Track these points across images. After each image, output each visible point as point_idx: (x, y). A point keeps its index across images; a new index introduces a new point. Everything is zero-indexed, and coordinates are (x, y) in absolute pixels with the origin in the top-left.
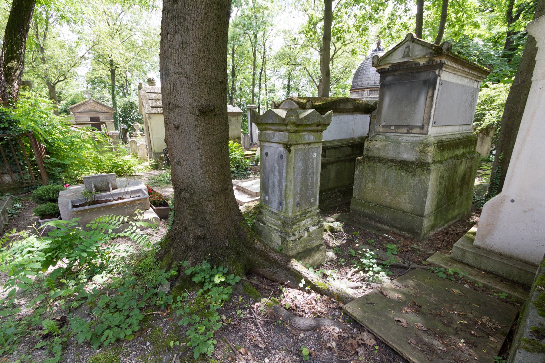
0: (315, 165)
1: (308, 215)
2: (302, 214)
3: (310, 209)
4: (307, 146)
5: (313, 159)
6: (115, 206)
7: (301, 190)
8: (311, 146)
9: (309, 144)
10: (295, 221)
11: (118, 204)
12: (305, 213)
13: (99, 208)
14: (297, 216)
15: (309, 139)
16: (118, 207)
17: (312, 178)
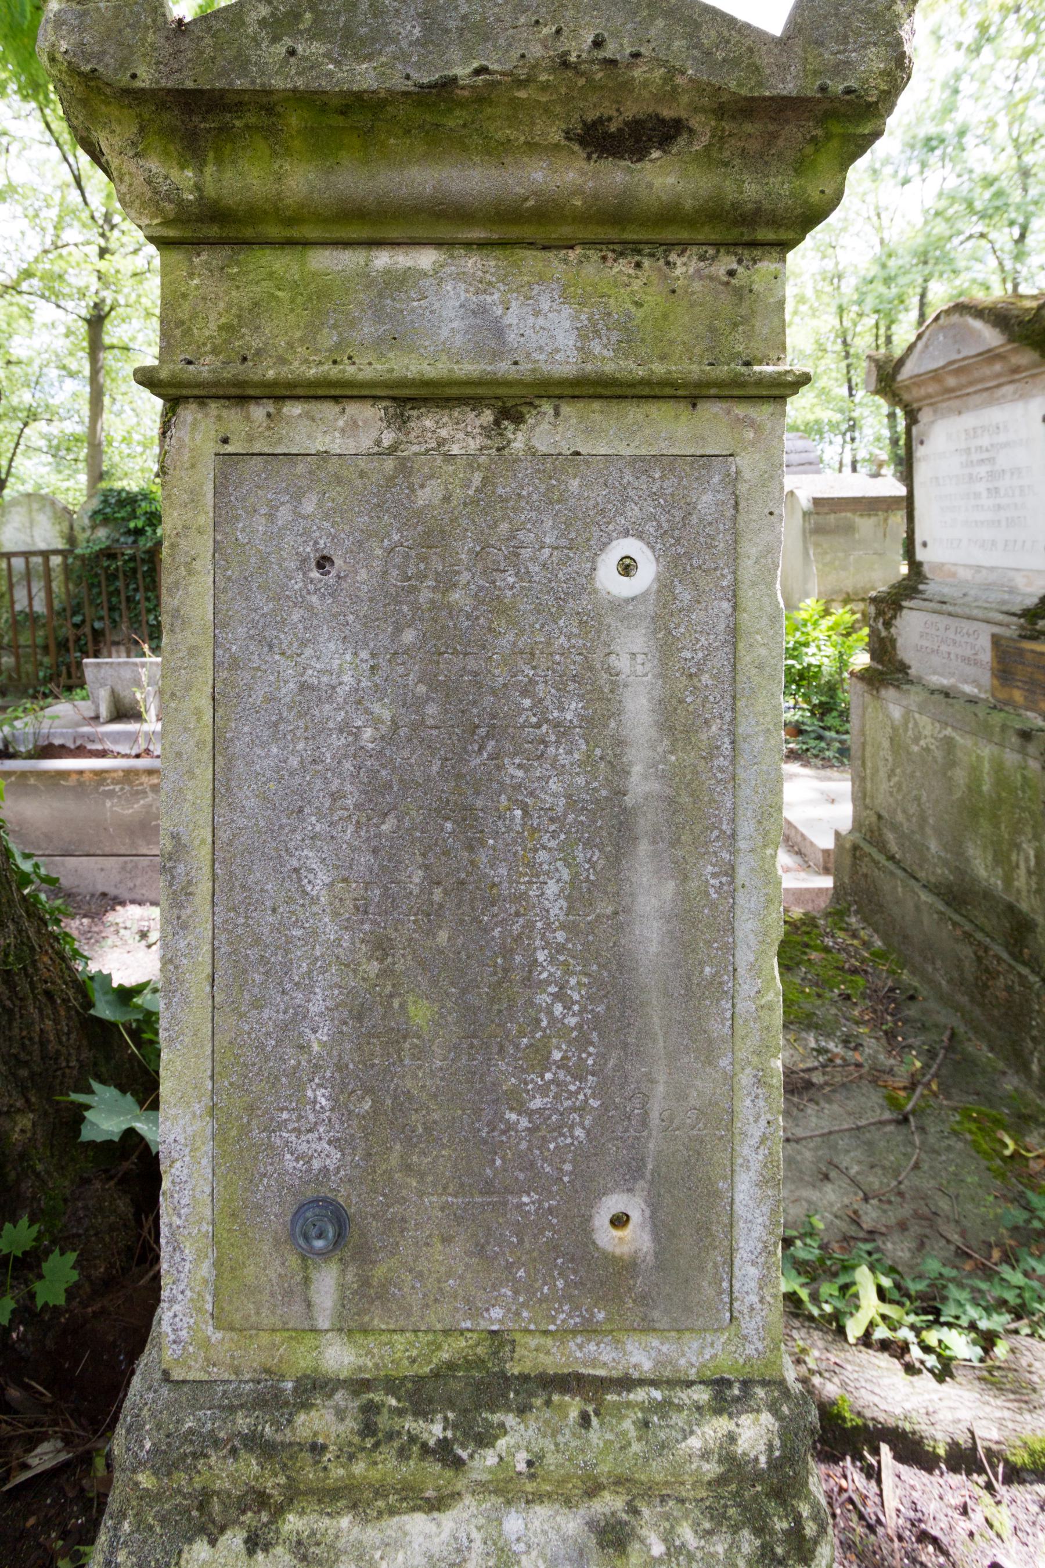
0: (638, 710)
1: (517, 1439)
2: (420, 1394)
3: (601, 1357)
4: (463, 434)
5: (597, 619)
6: (73, 780)
7: (371, 1021)
8: (545, 433)
9: (508, 402)
10: (230, 1473)
11: (81, 772)
12: (481, 1390)
13: (24, 775)
14: (315, 1387)
15: (491, 333)
16: (81, 784)
17: (599, 894)
